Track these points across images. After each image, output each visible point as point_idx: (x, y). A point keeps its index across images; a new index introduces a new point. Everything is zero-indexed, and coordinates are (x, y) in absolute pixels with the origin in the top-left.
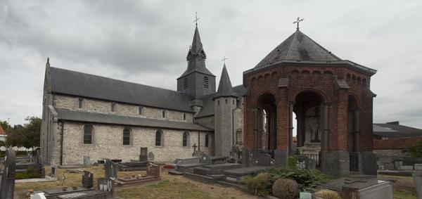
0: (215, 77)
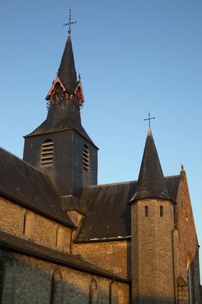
0: (98, 149)
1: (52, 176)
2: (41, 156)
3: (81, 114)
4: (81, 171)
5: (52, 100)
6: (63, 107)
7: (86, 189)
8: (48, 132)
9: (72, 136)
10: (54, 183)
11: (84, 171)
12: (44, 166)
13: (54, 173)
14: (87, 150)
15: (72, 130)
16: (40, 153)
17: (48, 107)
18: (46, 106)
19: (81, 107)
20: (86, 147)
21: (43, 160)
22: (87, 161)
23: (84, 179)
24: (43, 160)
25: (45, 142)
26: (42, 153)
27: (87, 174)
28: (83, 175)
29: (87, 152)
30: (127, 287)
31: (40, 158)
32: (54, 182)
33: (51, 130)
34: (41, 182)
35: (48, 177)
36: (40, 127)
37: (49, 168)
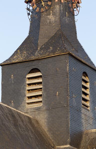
1: (42, 120)
2: (27, 92)
3: (77, 24)
4: (79, 111)
5: (35, 6)
6: (51, 17)
7: (87, 134)
8: (33, 58)
9: (68, 65)
10: (46, 130)
11: (83, 110)
12: (32, 107)
13: (46, 116)
14: (87, 79)
15: (68, 56)
16: (24, 89)
17: (29, 14)
18: (26, 12)
19: (76, 13)
20: (85, 74)
21: (30, 98)
22: (86, 94)
23: (83, 121)
24: (30, 98)
25: (31, 72)
26: (28, 88)
27: (88, 113)
28: (83, 116)
29: (86, 82)
30: (95, 72)
31: (25, 96)
32: (49, 135)
33: (37, 55)
34: (32, 132)
35: (37, 122)
36: (21, 49)
37: (38, 109)
